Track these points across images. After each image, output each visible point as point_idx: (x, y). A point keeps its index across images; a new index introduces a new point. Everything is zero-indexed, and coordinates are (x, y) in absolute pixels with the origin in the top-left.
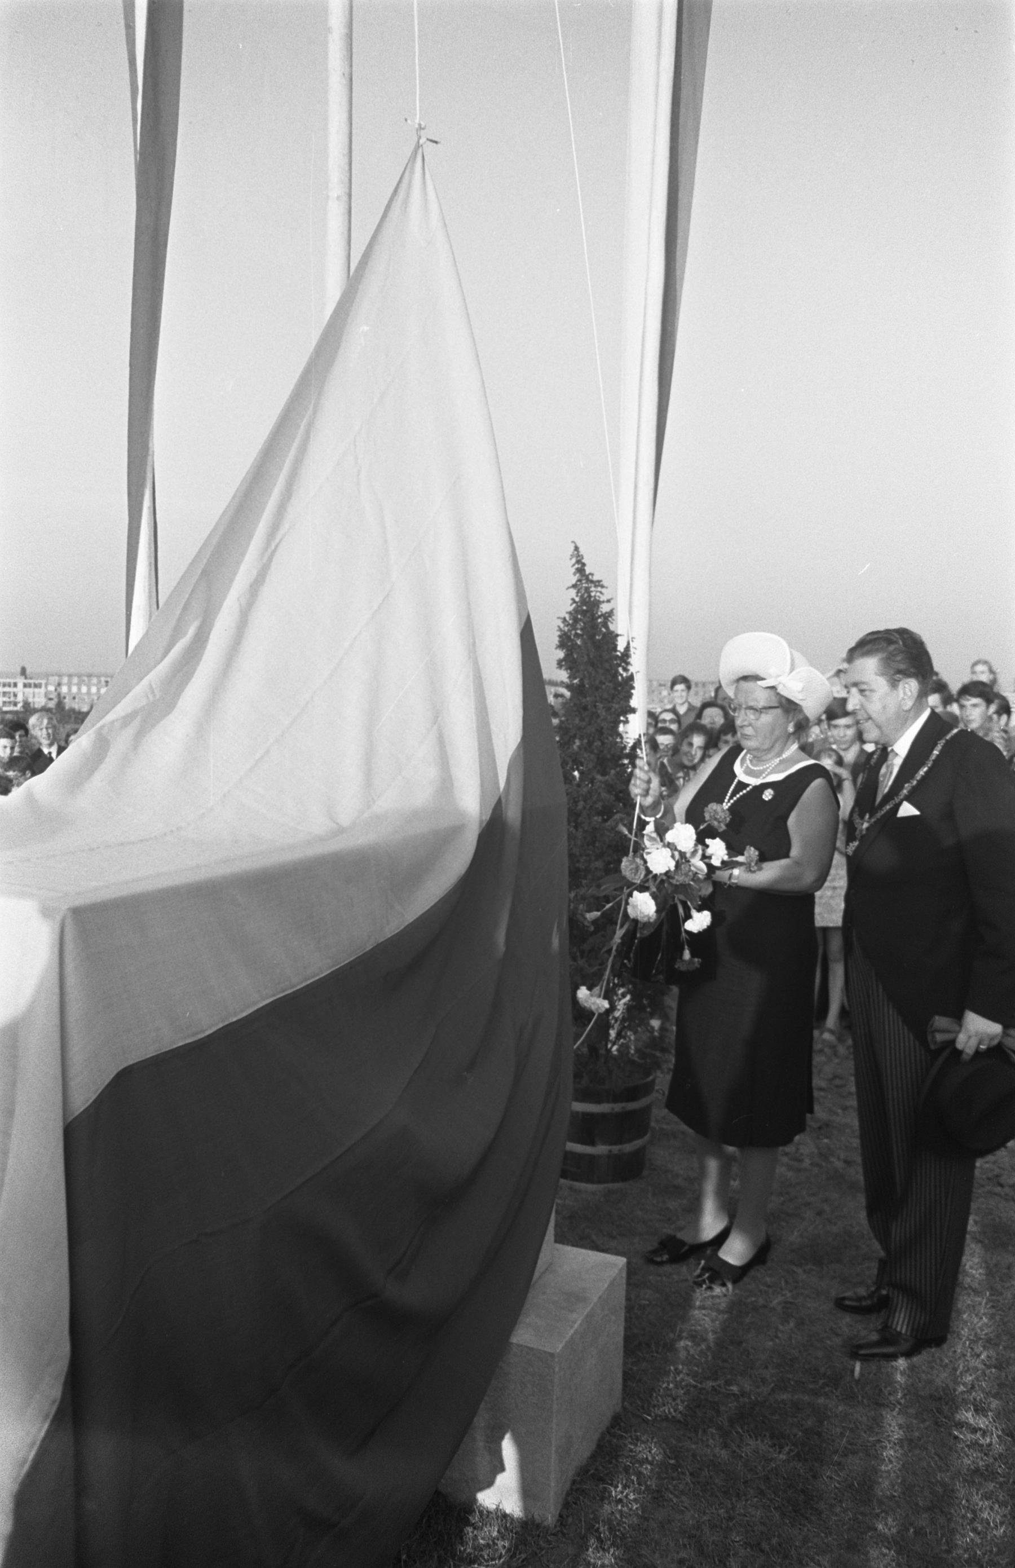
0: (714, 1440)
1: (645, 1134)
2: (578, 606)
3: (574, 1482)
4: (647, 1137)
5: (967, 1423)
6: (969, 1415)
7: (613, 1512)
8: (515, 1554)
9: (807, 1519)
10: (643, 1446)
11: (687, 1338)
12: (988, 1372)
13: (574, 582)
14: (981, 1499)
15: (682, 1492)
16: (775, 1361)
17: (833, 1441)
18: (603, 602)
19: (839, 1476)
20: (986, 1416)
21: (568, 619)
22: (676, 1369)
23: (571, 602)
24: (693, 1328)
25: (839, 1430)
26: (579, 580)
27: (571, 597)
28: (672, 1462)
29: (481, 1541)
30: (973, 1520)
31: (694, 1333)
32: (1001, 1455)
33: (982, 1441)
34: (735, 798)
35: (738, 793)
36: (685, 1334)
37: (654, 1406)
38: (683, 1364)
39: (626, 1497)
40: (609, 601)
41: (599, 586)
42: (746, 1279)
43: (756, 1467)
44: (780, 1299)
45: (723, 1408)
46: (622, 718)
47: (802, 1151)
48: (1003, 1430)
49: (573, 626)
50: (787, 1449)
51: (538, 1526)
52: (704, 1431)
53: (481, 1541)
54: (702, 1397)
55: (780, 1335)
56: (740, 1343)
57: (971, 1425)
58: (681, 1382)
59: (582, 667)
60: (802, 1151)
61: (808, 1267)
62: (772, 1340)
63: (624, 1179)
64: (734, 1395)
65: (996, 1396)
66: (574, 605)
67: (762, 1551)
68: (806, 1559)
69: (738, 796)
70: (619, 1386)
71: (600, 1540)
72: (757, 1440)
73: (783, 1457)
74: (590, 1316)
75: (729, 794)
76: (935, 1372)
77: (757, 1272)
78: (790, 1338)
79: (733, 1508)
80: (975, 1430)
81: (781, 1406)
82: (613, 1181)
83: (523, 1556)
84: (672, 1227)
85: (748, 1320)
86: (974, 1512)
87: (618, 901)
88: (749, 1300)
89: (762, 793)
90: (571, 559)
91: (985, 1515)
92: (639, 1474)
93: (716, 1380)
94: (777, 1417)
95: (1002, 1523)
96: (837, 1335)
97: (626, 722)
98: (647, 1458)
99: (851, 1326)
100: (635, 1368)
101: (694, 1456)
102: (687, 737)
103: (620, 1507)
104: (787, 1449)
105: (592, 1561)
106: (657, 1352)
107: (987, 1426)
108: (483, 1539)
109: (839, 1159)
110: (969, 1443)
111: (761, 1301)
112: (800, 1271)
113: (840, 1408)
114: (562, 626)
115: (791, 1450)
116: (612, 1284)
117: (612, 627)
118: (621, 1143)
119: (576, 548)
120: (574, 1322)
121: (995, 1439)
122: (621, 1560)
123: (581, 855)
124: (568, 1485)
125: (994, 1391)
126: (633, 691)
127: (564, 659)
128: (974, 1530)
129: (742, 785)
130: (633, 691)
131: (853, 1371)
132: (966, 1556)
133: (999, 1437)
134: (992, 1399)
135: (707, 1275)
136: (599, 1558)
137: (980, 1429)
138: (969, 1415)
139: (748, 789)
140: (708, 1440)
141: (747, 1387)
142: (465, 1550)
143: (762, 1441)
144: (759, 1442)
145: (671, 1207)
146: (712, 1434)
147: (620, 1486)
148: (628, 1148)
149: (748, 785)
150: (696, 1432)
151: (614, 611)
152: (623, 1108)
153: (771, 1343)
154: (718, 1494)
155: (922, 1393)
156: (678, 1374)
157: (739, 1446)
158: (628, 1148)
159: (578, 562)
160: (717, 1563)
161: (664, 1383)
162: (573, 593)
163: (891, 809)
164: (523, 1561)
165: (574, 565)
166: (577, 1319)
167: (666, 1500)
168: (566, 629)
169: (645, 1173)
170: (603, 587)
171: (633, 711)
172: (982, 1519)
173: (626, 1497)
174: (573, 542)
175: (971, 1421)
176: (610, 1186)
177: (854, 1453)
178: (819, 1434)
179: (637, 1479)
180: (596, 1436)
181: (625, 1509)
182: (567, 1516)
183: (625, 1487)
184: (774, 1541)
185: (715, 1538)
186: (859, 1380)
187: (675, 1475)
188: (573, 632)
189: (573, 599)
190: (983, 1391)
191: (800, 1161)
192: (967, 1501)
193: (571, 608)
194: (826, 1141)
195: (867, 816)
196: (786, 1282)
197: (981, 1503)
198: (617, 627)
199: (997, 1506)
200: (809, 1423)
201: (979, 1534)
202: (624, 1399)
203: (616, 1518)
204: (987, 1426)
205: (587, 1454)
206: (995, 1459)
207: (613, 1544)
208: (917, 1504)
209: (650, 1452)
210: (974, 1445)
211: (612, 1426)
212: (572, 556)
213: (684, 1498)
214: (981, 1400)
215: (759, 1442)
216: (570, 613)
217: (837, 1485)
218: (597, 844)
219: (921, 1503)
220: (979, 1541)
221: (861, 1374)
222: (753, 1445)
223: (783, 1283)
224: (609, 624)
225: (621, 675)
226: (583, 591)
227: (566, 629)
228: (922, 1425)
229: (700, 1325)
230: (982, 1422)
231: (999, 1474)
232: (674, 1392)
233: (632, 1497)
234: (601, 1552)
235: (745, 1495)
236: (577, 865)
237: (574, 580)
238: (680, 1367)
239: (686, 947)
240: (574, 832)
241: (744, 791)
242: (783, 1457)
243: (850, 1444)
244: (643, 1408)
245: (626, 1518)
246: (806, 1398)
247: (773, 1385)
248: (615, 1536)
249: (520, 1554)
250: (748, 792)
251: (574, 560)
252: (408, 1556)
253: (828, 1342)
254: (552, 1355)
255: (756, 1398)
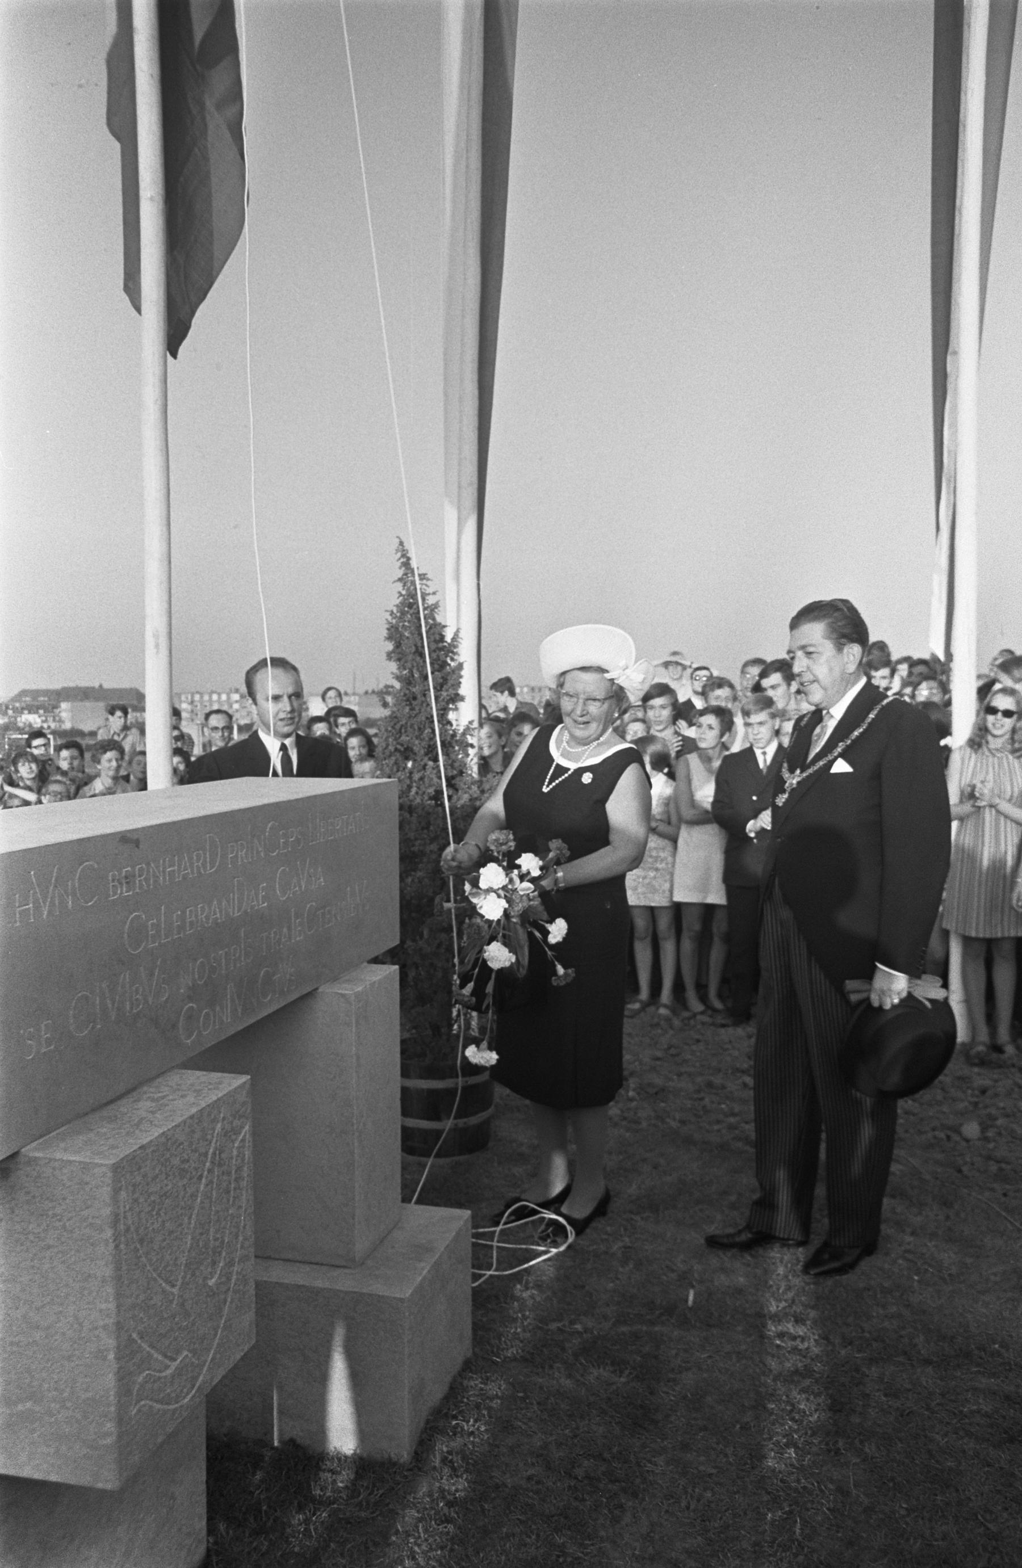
0: (560, 1372)
1: (490, 1105)
2: (405, 599)
3: (428, 1422)
4: (491, 1110)
5: (787, 1333)
6: (790, 1326)
7: (465, 1444)
8: (373, 1491)
9: (645, 1429)
10: (493, 1384)
11: (533, 1288)
12: (807, 1288)
13: (400, 576)
14: (799, 1393)
15: (530, 1419)
16: (616, 1299)
17: (669, 1361)
18: (429, 594)
19: (674, 1390)
20: (804, 1325)
21: (395, 611)
22: (523, 1315)
23: (398, 595)
24: (539, 1278)
25: (674, 1352)
26: (406, 574)
27: (397, 590)
28: (521, 1395)
29: (341, 1485)
30: (791, 1411)
31: (539, 1283)
32: (817, 1356)
33: (801, 1347)
34: (554, 784)
35: (554, 781)
36: (531, 1285)
37: (503, 1350)
38: (529, 1311)
39: (478, 1429)
40: (434, 593)
41: (424, 579)
42: (588, 1231)
43: (599, 1391)
44: (620, 1244)
45: (567, 1345)
46: (451, 706)
47: (639, 1115)
48: (819, 1335)
49: (401, 618)
50: (627, 1372)
51: (395, 1464)
52: (551, 1367)
53: (341, 1485)
54: (548, 1337)
55: (620, 1276)
56: (583, 1287)
57: (791, 1334)
58: (527, 1326)
59: (410, 657)
60: (639, 1115)
61: (646, 1214)
62: (613, 1282)
63: (471, 1151)
64: (578, 1332)
65: (813, 1308)
66: (401, 598)
67: (604, 1460)
68: (644, 1461)
69: (557, 782)
70: (468, 1332)
71: (454, 1469)
72: (599, 1368)
73: (623, 1380)
74: (437, 1265)
75: (547, 780)
76: (760, 1293)
77: (599, 1223)
78: (630, 1278)
79: (578, 1428)
80: (794, 1338)
81: (622, 1337)
82: (460, 1154)
83: (381, 1492)
84: (518, 1190)
85: (589, 1266)
86: (793, 1405)
87: (461, 1063)
88: (591, 1248)
89: (581, 776)
90: (396, 553)
91: (802, 1407)
92: (489, 1409)
93: (560, 1321)
94: (617, 1347)
95: (816, 1410)
96: (673, 1271)
97: (456, 709)
98: (497, 1394)
99: (685, 1261)
100: (484, 1319)
101: (541, 1388)
102: (515, 726)
103: (472, 1439)
104: (627, 1372)
105: (447, 1488)
106: (506, 1303)
107: (805, 1333)
108: (342, 1482)
109: (674, 1119)
110: (789, 1349)
111: (603, 1247)
112: (638, 1218)
113: (676, 1333)
114: (389, 618)
115: (630, 1373)
116: (458, 1234)
117: (439, 619)
118: (466, 1116)
119: (401, 543)
120: (423, 1269)
121: (812, 1343)
122: (474, 1483)
123: (416, 839)
124: (422, 1425)
125: (812, 1303)
126: (461, 680)
127: (393, 652)
128: (793, 1419)
129: (561, 770)
130: (461, 680)
131: (687, 1301)
132: (785, 1440)
133: (815, 1340)
134: (809, 1310)
135: (551, 1229)
136: (454, 1484)
137: (799, 1336)
138: (790, 1326)
139: (570, 772)
140: (554, 1373)
141: (590, 1325)
142: (324, 1494)
143: (604, 1369)
144: (601, 1370)
145: (517, 1174)
146: (558, 1368)
147: (472, 1420)
148: (474, 1120)
149: (569, 769)
150: (543, 1368)
151: (440, 604)
152: (465, 1123)
153: (611, 1285)
154: (565, 1418)
155: (748, 1312)
156: (526, 1320)
157: (582, 1375)
158: (474, 1120)
159: (403, 556)
160: (563, 1474)
161: (511, 1328)
162: (399, 586)
163: (825, 765)
164: (381, 1496)
165: (399, 559)
166: (425, 1268)
167: (515, 1428)
168: (394, 621)
169: (491, 1144)
170: (428, 579)
171: (462, 699)
172: (800, 1409)
173: (478, 1429)
174: (398, 537)
175: (792, 1331)
176: (456, 1158)
177: (688, 1369)
178: (656, 1357)
179: (488, 1413)
180: (448, 1379)
181: (477, 1440)
182: (422, 1453)
183: (476, 1421)
184: (615, 1450)
185: (561, 1454)
186: (693, 1307)
187: (523, 1406)
188: (401, 624)
189: (399, 592)
190: (803, 1305)
191: (640, 1123)
192: (787, 1396)
193: (398, 601)
194: (663, 1105)
195: (798, 771)
196: (626, 1229)
197: (799, 1396)
198: (445, 617)
199: (812, 1397)
200: (647, 1349)
201: (797, 1421)
202: (474, 1347)
203: (469, 1449)
204: (805, 1333)
205: (439, 1395)
206: (813, 1359)
207: (467, 1471)
208: (743, 1406)
209: (500, 1389)
210: (795, 1350)
211: (463, 1370)
212: (397, 551)
213: (532, 1424)
214: (801, 1312)
215: (601, 1370)
216: (397, 606)
217: (673, 1398)
218: (432, 828)
219: (746, 1404)
220: (796, 1427)
221: (694, 1302)
222: (596, 1374)
223: (622, 1232)
224: (436, 615)
225: (449, 665)
226: (409, 585)
227: (394, 621)
228: (748, 1340)
229: (545, 1275)
230: (801, 1331)
231: (814, 1371)
232: (521, 1336)
233: (483, 1428)
234: (455, 1479)
235: (589, 1415)
236: (412, 849)
237: (400, 573)
238: (527, 1313)
239: (556, 963)
240: (408, 816)
241: (566, 775)
242: (623, 1380)
243: (685, 1362)
244: (492, 1352)
245: (478, 1447)
246: (645, 1328)
247: (614, 1319)
248: (468, 1464)
249: (378, 1490)
250: (569, 775)
251: (399, 554)
252: (269, 1507)
253: (665, 1278)
254: (401, 1300)
255: (598, 1333)
